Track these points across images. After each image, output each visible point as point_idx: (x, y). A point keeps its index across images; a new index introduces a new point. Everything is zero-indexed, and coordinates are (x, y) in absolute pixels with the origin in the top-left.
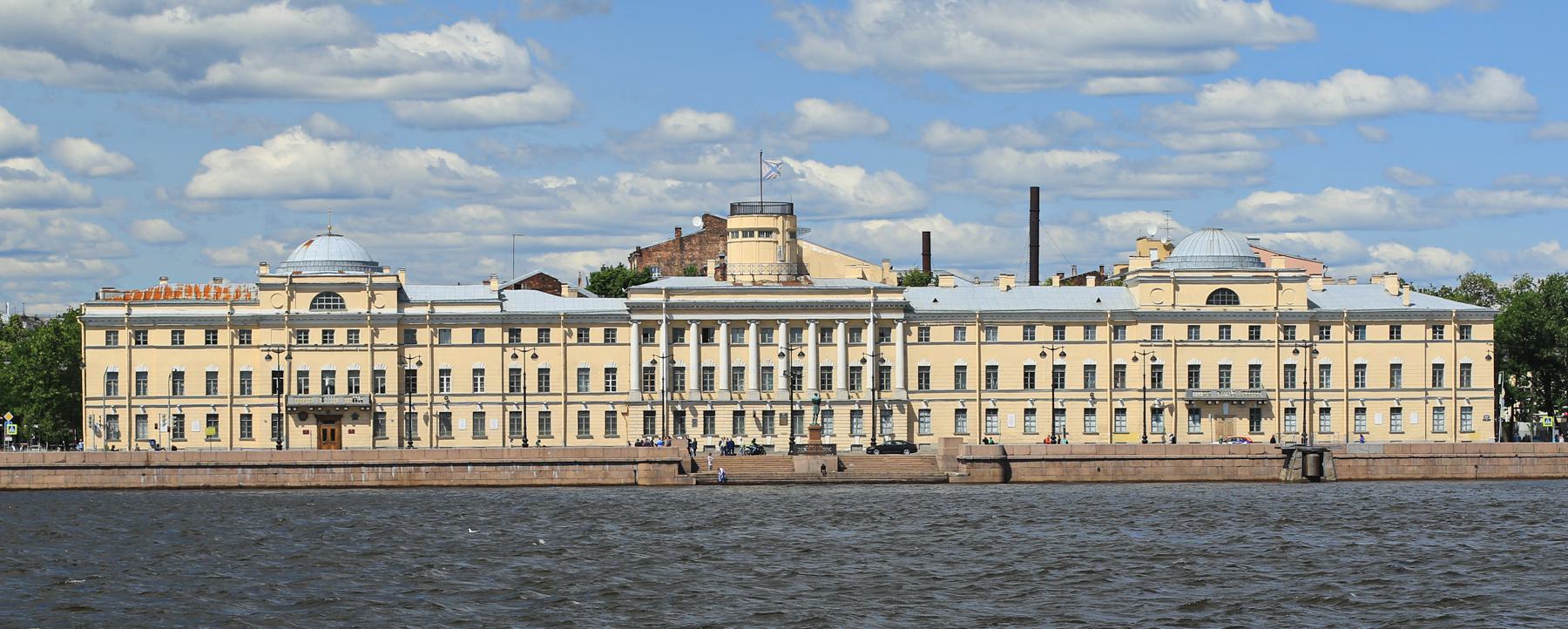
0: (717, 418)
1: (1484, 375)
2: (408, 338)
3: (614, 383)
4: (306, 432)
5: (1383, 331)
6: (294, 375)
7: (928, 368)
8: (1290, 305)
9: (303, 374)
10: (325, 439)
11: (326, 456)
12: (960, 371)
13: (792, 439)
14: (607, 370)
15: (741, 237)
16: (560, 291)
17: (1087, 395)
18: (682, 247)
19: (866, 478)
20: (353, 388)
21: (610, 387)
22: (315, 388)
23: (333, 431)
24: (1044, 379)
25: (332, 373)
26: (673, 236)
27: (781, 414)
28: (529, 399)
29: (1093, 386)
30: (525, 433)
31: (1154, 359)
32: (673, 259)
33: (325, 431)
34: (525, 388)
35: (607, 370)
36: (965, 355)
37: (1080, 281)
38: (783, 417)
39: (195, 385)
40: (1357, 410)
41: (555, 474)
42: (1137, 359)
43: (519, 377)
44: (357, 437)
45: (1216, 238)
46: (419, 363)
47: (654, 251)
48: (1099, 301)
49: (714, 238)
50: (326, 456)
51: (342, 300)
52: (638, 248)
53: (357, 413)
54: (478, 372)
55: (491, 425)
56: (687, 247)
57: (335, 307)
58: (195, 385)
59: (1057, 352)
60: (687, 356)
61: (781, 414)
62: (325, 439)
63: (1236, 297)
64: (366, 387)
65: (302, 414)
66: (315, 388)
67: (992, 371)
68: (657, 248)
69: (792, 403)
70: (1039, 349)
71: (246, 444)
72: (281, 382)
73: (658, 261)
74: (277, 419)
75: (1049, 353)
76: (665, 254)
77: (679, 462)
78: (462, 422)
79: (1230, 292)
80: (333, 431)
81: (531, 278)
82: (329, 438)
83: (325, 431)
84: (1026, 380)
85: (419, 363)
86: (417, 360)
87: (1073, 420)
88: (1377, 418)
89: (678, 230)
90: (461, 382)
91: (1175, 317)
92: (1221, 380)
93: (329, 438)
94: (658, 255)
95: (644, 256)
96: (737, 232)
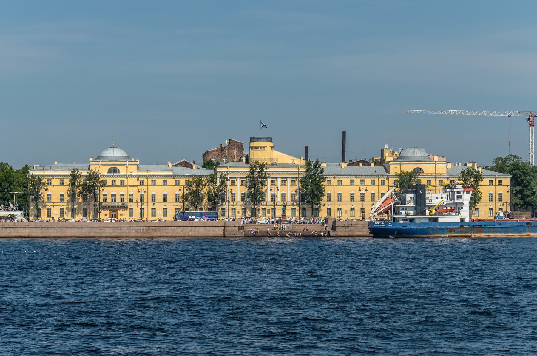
0: (277, 210)
1: (506, 197)
8: (440, 173)
9: (105, 195)
15: (254, 149)
17: (372, 203)
20: (122, 200)
22: (109, 200)
23: (115, 215)
24: (357, 198)
25: (115, 195)
27: (268, 210)
29: (155, 201)
30: (100, 217)
31: (231, 192)
32: (219, 155)
33: (112, 215)
34: (100, 200)
37: (357, 164)
40: (338, 209)
41: (197, 231)
42: (360, 190)
43: (285, 197)
45: (415, 150)
46: (145, 192)
47: (212, 152)
48: (376, 171)
49: (233, 147)
51: (118, 170)
53: (124, 208)
55: (158, 213)
57: (116, 172)
59: (364, 189)
61: (268, 210)
66: (109, 200)
68: (213, 151)
73: (214, 155)
76: (216, 153)
77: (239, 226)
79: (421, 169)
80: (115, 215)
81: (181, 163)
83: (112, 215)
84: (351, 198)
85: (145, 192)
86: (144, 190)
89: (221, 145)
92: (490, 199)
94: (214, 153)
95: (209, 154)
96: (253, 148)
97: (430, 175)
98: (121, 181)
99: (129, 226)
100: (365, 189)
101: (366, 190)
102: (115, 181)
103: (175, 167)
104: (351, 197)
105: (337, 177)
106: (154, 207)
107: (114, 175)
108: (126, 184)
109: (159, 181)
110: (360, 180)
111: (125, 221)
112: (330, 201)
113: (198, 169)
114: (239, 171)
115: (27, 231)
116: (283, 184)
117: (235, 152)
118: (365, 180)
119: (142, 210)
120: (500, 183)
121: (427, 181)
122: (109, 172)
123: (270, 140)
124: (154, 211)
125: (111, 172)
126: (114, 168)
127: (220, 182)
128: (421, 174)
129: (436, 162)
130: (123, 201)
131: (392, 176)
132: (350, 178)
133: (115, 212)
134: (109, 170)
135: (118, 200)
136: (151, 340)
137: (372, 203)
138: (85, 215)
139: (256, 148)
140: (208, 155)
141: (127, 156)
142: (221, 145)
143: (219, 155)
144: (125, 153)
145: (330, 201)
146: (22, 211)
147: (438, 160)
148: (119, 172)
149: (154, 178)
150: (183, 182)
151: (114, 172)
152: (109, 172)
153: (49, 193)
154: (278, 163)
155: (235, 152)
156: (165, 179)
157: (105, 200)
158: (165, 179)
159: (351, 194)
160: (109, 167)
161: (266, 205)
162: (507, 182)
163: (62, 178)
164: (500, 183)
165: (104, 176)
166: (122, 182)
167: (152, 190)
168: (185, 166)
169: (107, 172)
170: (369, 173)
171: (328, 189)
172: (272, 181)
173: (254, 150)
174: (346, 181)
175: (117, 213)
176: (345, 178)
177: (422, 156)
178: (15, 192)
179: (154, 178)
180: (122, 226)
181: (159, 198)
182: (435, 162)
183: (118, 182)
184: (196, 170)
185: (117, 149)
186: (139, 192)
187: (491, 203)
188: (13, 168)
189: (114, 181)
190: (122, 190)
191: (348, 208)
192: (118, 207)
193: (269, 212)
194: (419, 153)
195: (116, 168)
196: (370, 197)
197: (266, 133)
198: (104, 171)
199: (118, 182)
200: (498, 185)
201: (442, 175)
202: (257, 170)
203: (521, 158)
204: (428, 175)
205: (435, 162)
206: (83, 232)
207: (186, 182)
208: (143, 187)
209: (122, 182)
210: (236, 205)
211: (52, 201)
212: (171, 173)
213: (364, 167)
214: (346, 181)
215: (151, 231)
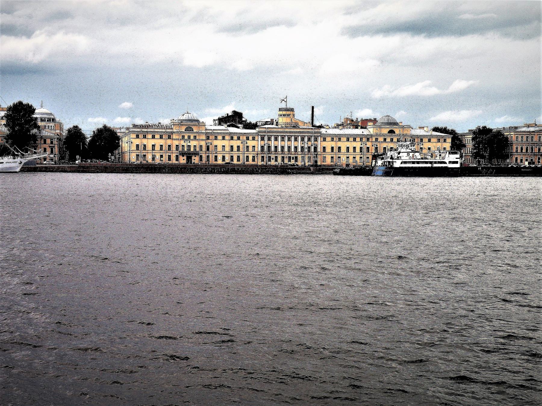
2: (208, 138)
3: (254, 149)
4: (184, 160)
5: (345, 139)
7: (349, 147)
12: (332, 148)
14: (253, 146)
20: (195, 149)
21: (254, 150)
28: (243, 153)
35: (153, 145)
36: (333, 144)
38: (293, 158)
39: (157, 148)
54: (224, 146)
57: (191, 130)
58: (157, 148)
60: (273, 143)
63: (395, 132)
64: (198, 149)
65: (183, 154)
67: (339, 148)
70: (241, 141)
71: (248, 163)
74: (177, 156)
75: (374, 145)
78: (220, 158)
87: (358, 158)
88: (286, 161)
89: (228, 114)
90: (220, 149)
91: (380, 135)
101: (211, 144)
108: (197, 138)
112: (333, 152)
119: (208, 157)
120: (445, 141)
125: (187, 130)
126: (189, 127)
142: (228, 114)
145: (333, 152)
148: (193, 130)
151: (189, 130)
153: (248, 145)
159: (354, 147)
161: (291, 154)
162: (449, 140)
164: (445, 141)
166: (195, 137)
172: (302, 138)
173: (282, 116)
187: (332, 153)
188: (475, 129)
189: (189, 137)
191: (352, 156)
195: (191, 127)
199: (192, 137)
208: (210, 141)
209: (195, 137)
210: (278, 154)
211: (147, 149)
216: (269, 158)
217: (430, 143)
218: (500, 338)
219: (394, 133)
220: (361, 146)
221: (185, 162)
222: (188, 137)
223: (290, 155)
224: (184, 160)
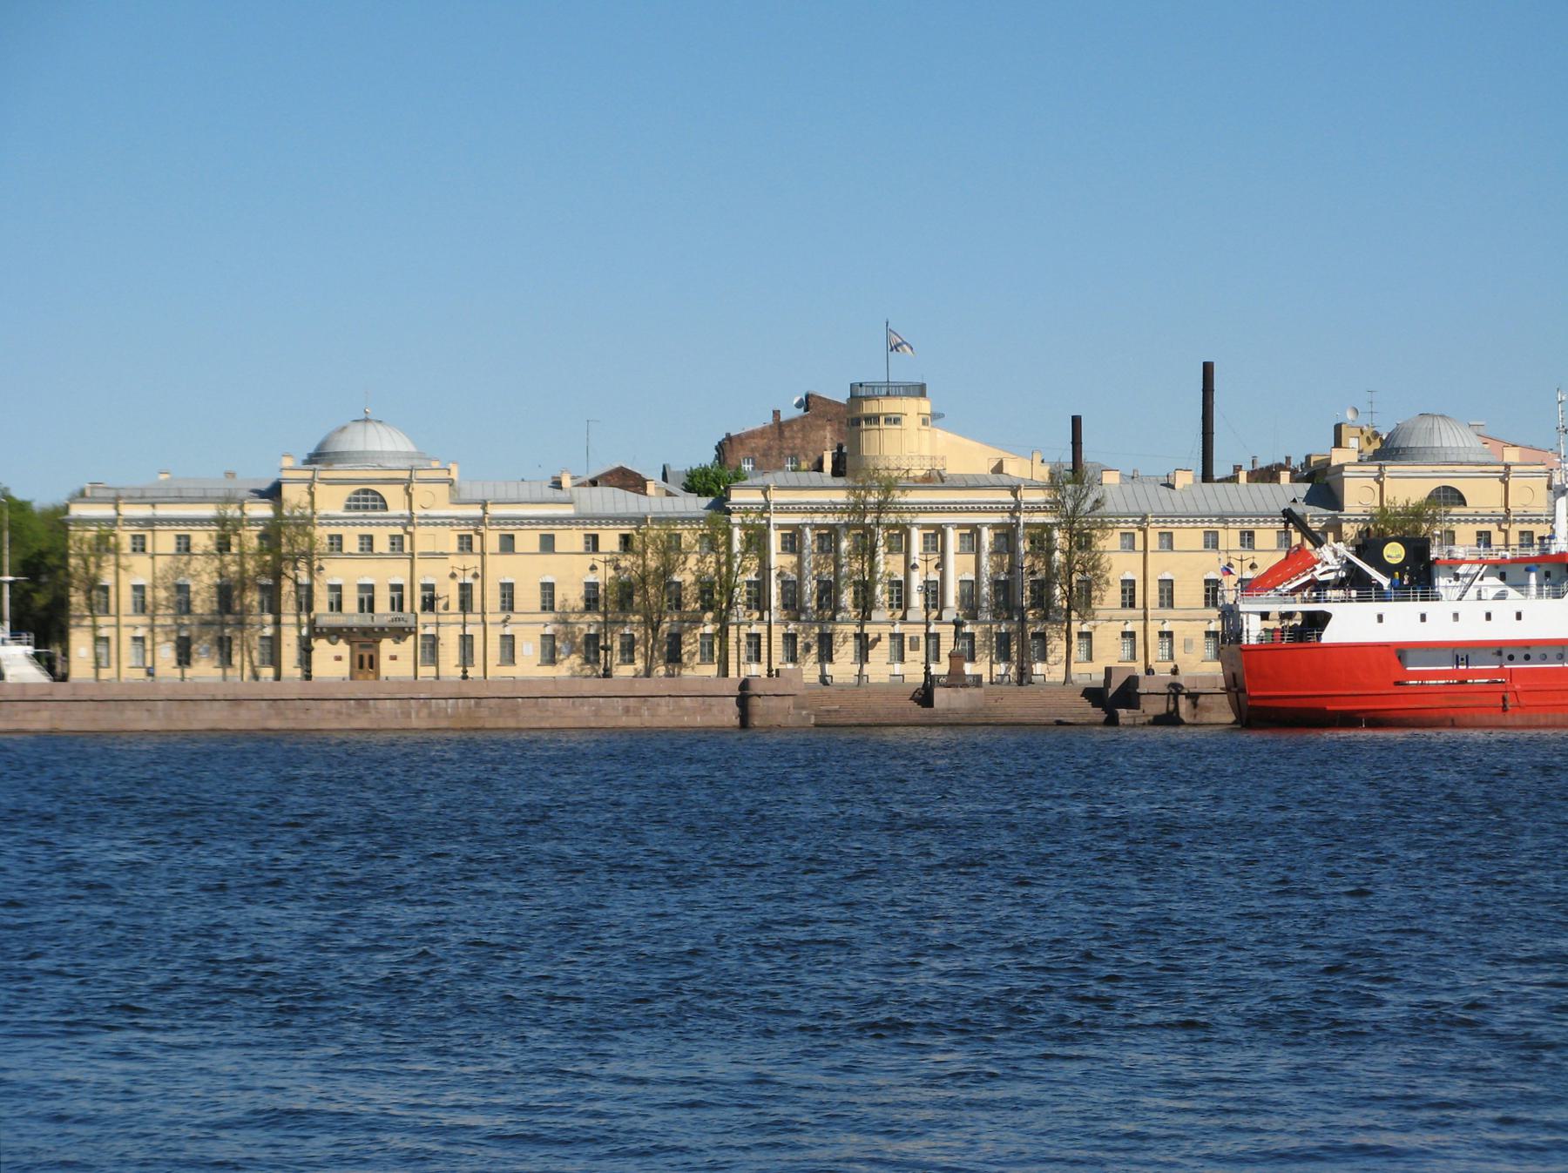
4: (339, 658)
6: (418, 589)
9: (336, 589)
10: (361, 666)
11: (362, 688)
13: (927, 668)
16: (645, 487)
18: (781, 433)
19: (1007, 719)
20: (397, 604)
22: (351, 604)
23: (371, 658)
25: (371, 588)
26: (770, 420)
27: (911, 638)
32: (770, 448)
33: (361, 658)
44: (396, 660)
45: (1436, 426)
49: (819, 422)
50: (362, 688)
51: (383, 500)
52: (728, 435)
53: (399, 634)
56: (787, 434)
57: (375, 508)
59: (1247, 564)
61: (911, 639)
62: (361, 666)
65: (334, 634)
66: (351, 604)
69: (438, 624)
71: (508, 671)
72: (401, 598)
76: (762, 443)
80: (371, 658)
81: (610, 474)
82: (366, 663)
83: (361, 658)
84: (1207, 597)
86: (472, 572)
89: (776, 413)
93: (366, 663)
97: (1488, 511)
98: (362, 537)
99: (406, 696)
100: (1250, 562)
102: (340, 537)
103: (586, 491)
104: (1207, 590)
105: (1157, 522)
106: (508, 631)
107: (365, 517)
109: (527, 540)
110: (1238, 532)
111: (262, 680)
113: (669, 494)
114: (808, 503)
115: (45, 714)
116: (930, 545)
117: (828, 440)
118: (1257, 532)
121: (1479, 534)
122: (348, 508)
123: (920, 391)
124: (509, 642)
125: (357, 508)
126: (366, 492)
127: (741, 542)
128: (1455, 510)
129: (1507, 466)
130: (371, 610)
131: (1353, 518)
132: (1199, 525)
133: (370, 646)
134: (349, 500)
135: (382, 605)
136: (774, 1064)
137: (503, 616)
138: (226, 661)
139: (887, 421)
140: (732, 451)
141: (412, 449)
142: (776, 413)
143: (770, 448)
144: (407, 440)
146: (28, 644)
147: (1517, 460)
148: (385, 508)
149: (509, 529)
150: (610, 540)
151: (366, 508)
152: (348, 508)
154: (948, 472)
155: (828, 440)
156: (545, 529)
157: (337, 606)
158: (545, 529)
160: (349, 490)
163: (182, 530)
165: (329, 520)
167: (501, 569)
168: (620, 487)
169: (342, 507)
170: (1224, 509)
171: (1119, 563)
174: (1189, 537)
175: (378, 651)
176: (1184, 525)
177: (1461, 445)
178: (10, 578)
179: (509, 529)
180: (382, 696)
181: (529, 598)
182: (1502, 468)
183: (382, 544)
184: (658, 500)
185: (379, 427)
186: (453, 576)
189: (368, 542)
190: (397, 572)
192: (382, 629)
193: (914, 646)
194: (1451, 433)
196: (1203, 592)
197: (903, 372)
198: (331, 501)
199: (382, 544)
200: (497, 550)
201: (1531, 511)
202: (871, 499)
203: (1388, 451)
204: (1481, 511)
205: (1502, 468)
206: (245, 719)
207: (461, 543)
209: (397, 542)
212: (567, 511)
213: (1253, 486)
214: (1189, 537)
215: (484, 712)
216: (749, 644)
217: (1169, 555)
218: (24, 1153)
219: (1461, 500)
220: (591, 578)
221: (344, 668)
222: (393, 544)
223: (898, 629)
224: (339, 658)
